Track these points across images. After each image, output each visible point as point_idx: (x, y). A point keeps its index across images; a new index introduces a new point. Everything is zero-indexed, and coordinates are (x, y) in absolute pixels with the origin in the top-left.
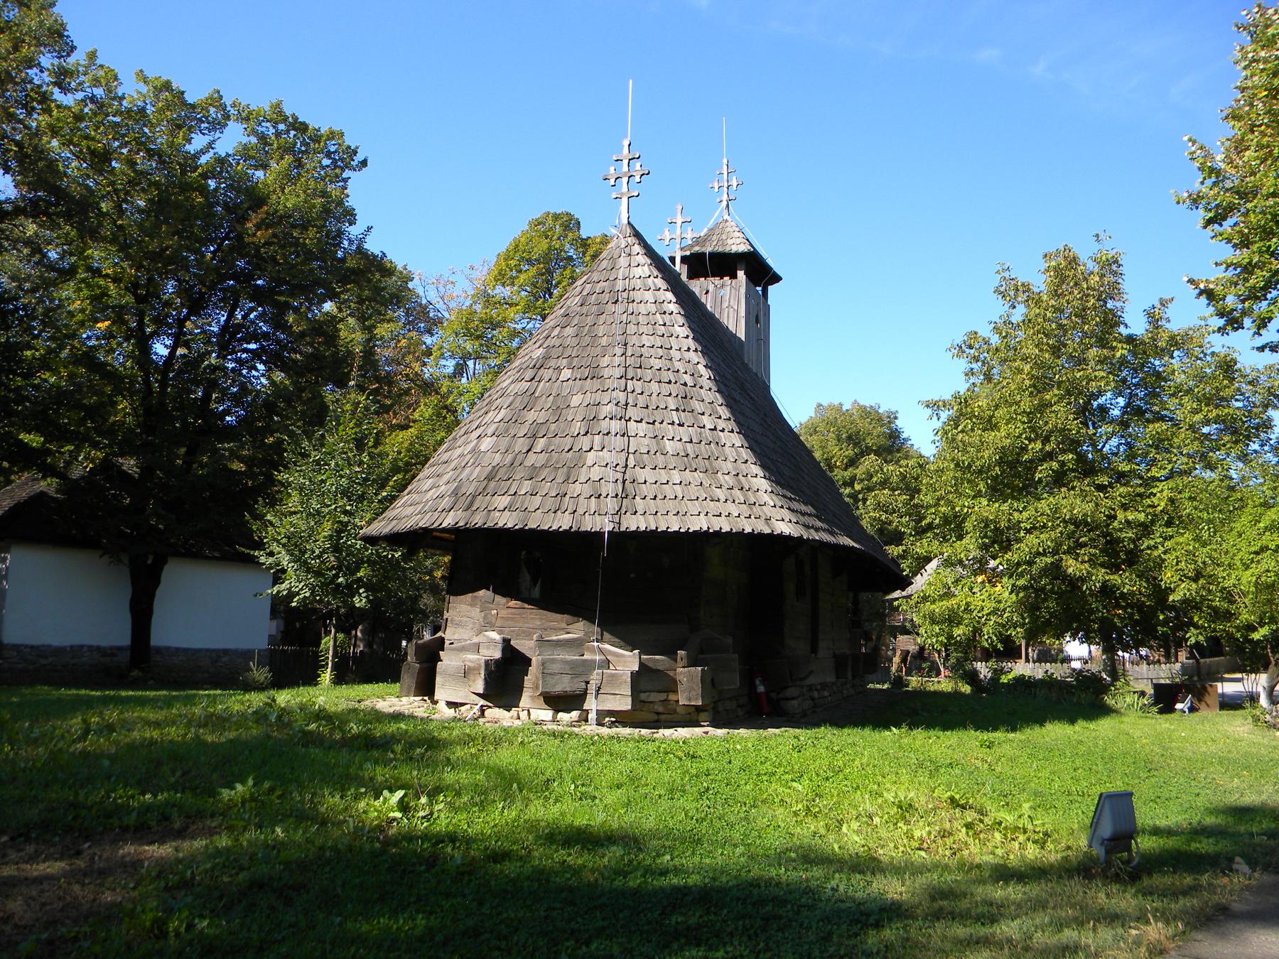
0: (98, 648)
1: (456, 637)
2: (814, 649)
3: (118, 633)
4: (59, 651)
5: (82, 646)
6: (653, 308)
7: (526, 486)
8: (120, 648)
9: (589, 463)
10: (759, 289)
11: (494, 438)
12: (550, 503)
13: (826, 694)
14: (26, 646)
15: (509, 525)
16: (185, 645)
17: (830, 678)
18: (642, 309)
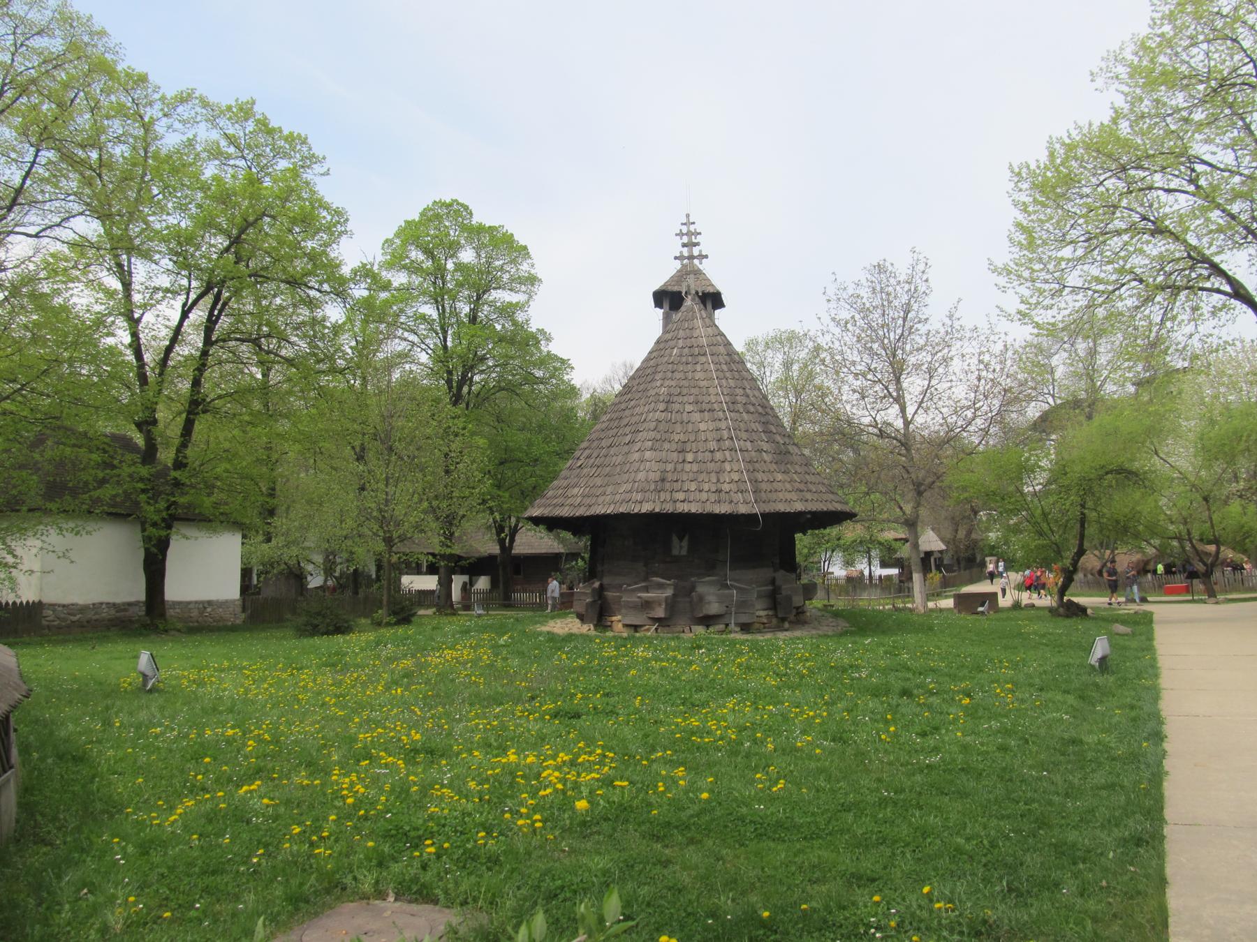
0: (114, 604)
4: (83, 609)
7: (693, 486)
8: (136, 604)
12: (713, 497)
16: (194, 599)
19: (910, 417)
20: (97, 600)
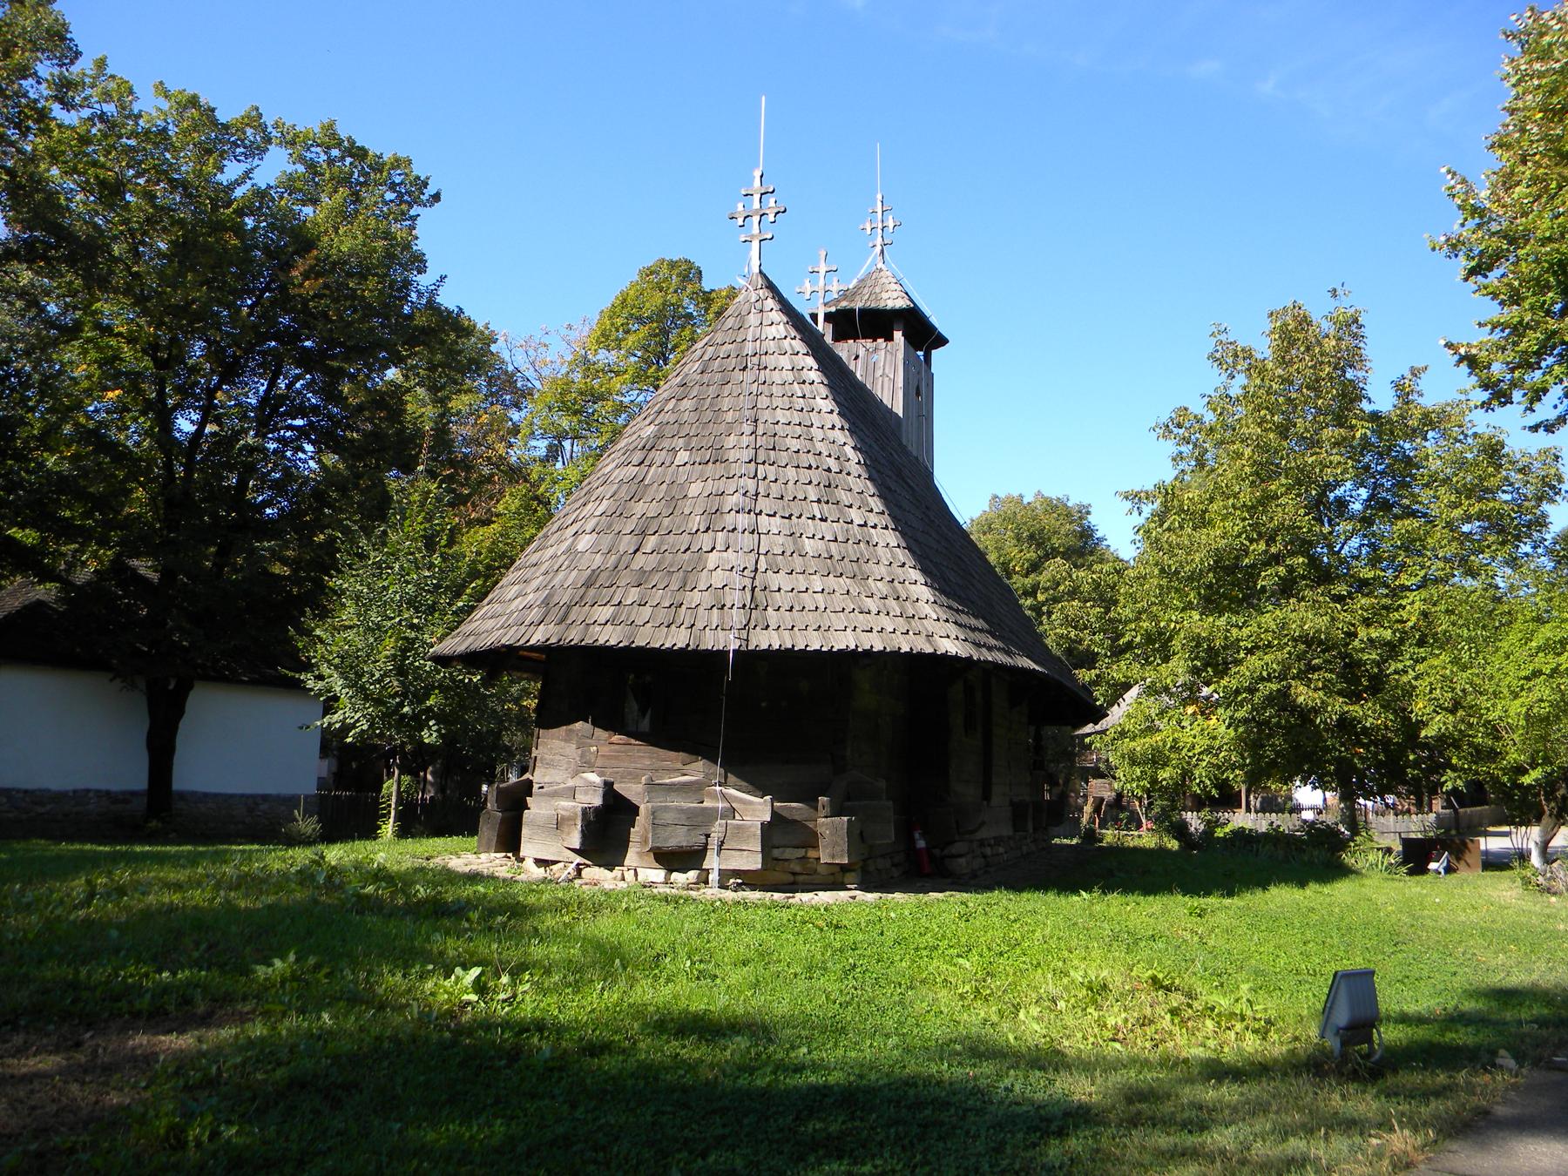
0: (108, 793)
1: (547, 779)
2: (987, 796)
3: (132, 775)
4: (60, 797)
5: (88, 791)
6: (790, 376)
7: (634, 595)
8: (134, 794)
9: (711, 566)
10: (920, 353)
11: (594, 535)
12: (663, 615)
13: (1001, 850)
14: (18, 791)
15: (612, 642)
17: (1006, 831)
18: (777, 377)
19: (905, 616)
20: (80, 784)
